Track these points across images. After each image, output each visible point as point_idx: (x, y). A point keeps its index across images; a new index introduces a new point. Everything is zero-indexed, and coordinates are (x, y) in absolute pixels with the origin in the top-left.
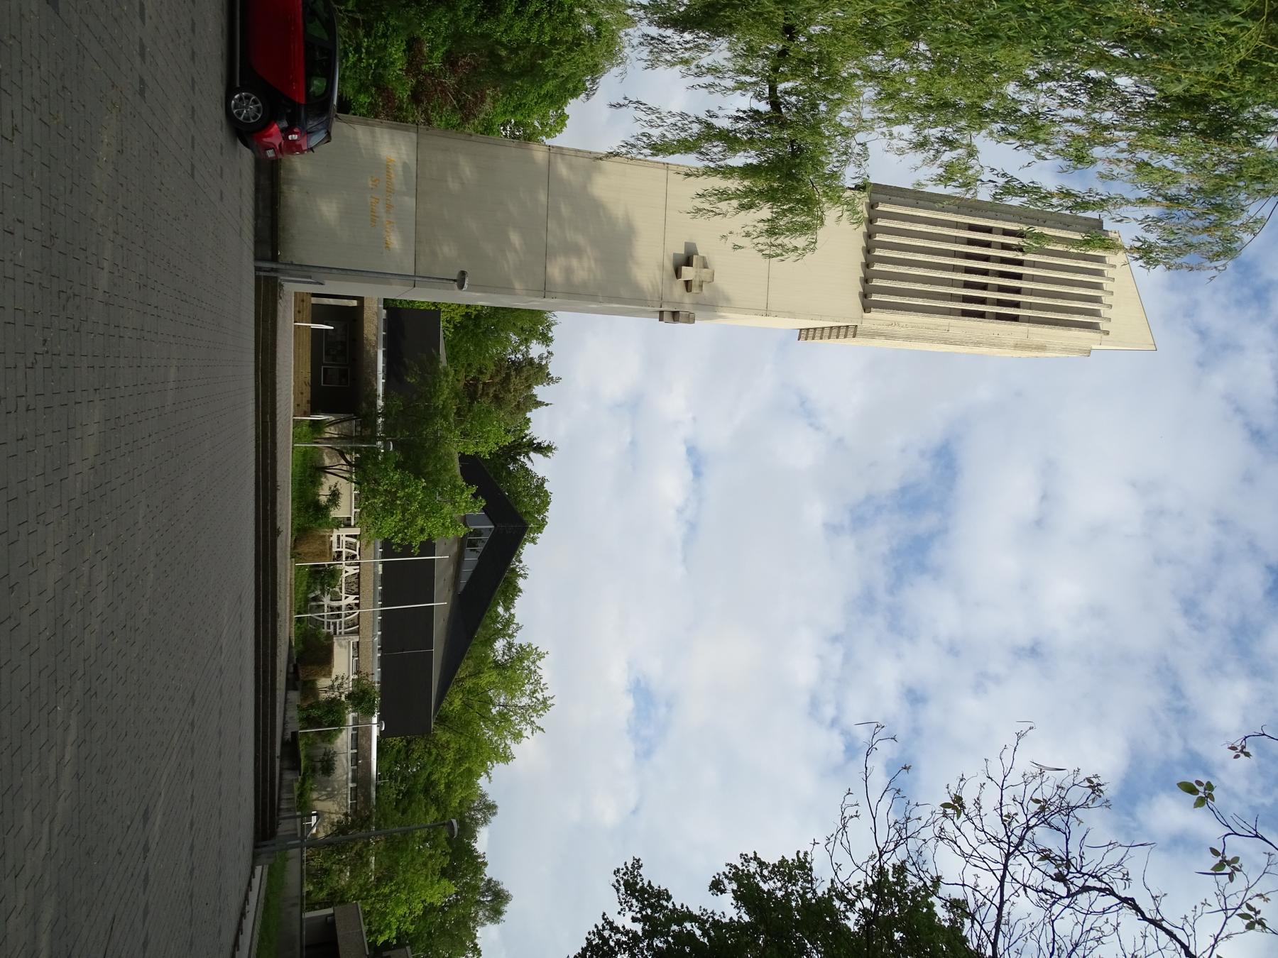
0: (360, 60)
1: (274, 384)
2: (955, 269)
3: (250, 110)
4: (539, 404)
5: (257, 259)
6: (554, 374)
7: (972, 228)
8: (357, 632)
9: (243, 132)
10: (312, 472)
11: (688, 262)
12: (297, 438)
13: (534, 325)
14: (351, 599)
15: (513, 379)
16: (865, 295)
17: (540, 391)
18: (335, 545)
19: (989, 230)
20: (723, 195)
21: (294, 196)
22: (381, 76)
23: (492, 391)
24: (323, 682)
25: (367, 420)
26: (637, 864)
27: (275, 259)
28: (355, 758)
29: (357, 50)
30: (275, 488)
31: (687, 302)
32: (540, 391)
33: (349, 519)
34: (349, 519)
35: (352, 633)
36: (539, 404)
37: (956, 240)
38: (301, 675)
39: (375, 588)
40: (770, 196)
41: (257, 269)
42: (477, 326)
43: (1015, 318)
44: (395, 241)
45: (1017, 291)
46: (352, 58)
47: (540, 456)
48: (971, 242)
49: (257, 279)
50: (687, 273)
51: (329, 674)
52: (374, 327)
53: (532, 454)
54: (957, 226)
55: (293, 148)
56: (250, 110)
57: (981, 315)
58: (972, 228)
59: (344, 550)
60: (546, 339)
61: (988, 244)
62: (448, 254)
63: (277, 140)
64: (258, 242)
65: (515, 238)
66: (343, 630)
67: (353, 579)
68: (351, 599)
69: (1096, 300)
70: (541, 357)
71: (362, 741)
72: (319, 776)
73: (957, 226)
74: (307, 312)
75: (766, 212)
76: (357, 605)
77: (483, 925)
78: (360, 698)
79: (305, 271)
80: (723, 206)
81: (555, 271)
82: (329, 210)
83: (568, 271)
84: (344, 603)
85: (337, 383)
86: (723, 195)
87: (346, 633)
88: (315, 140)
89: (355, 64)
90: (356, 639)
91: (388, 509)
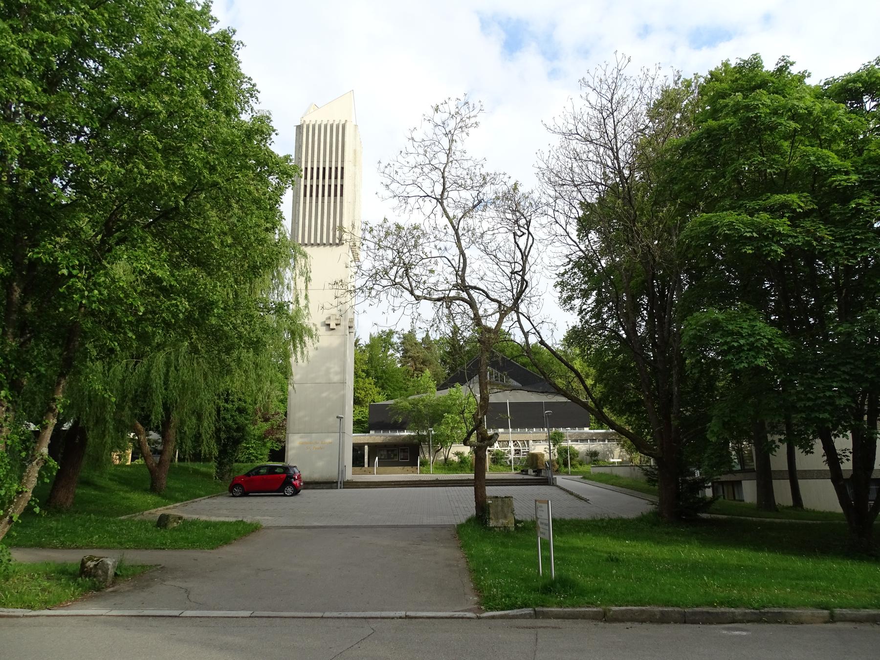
1: (800, 499)
2: (323, 202)
3: (290, 490)
7: (305, 195)
8: (528, 441)
9: (296, 492)
10: (447, 464)
11: (329, 325)
12: (428, 472)
14: (511, 444)
16: (337, 245)
19: (305, 186)
20: (302, 353)
21: (317, 476)
22: (259, 437)
23: (418, 366)
24: (547, 457)
25: (422, 439)
27: (337, 482)
28: (592, 440)
29: (248, 448)
31: (345, 324)
37: (311, 202)
40: (301, 337)
42: (381, 378)
43: (342, 168)
44: (329, 440)
45: (330, 169)
46: (252, 451)
48: (311, 195)
50: (333, 326)
51: (543, 455)
52: (375, 437)
54: (305, 203)
55: (299, 477)
56: (290, 490)
57: (342, 186)
58: (305, 195)
60: (391, 333)
61: (311, 186)
62: (332, 420)
63: (298, 482)
64: (332, 488)
65: (324, 395)
68: (511, 444)
69: (332, 126)
70: (399, 338)
71: (584, 437)
72: (600, 457)
73: (305, 203)
74: (370, 469)
75: (306, 338)
78: (555, 439)
79: (342, 471)
80: (305, 353)
81: (336, 378)
82: (320, 464)
83: (337, 373)
85: (406, 454)
86: (302, 353)
88: (296, 471)
90: (531, 442)
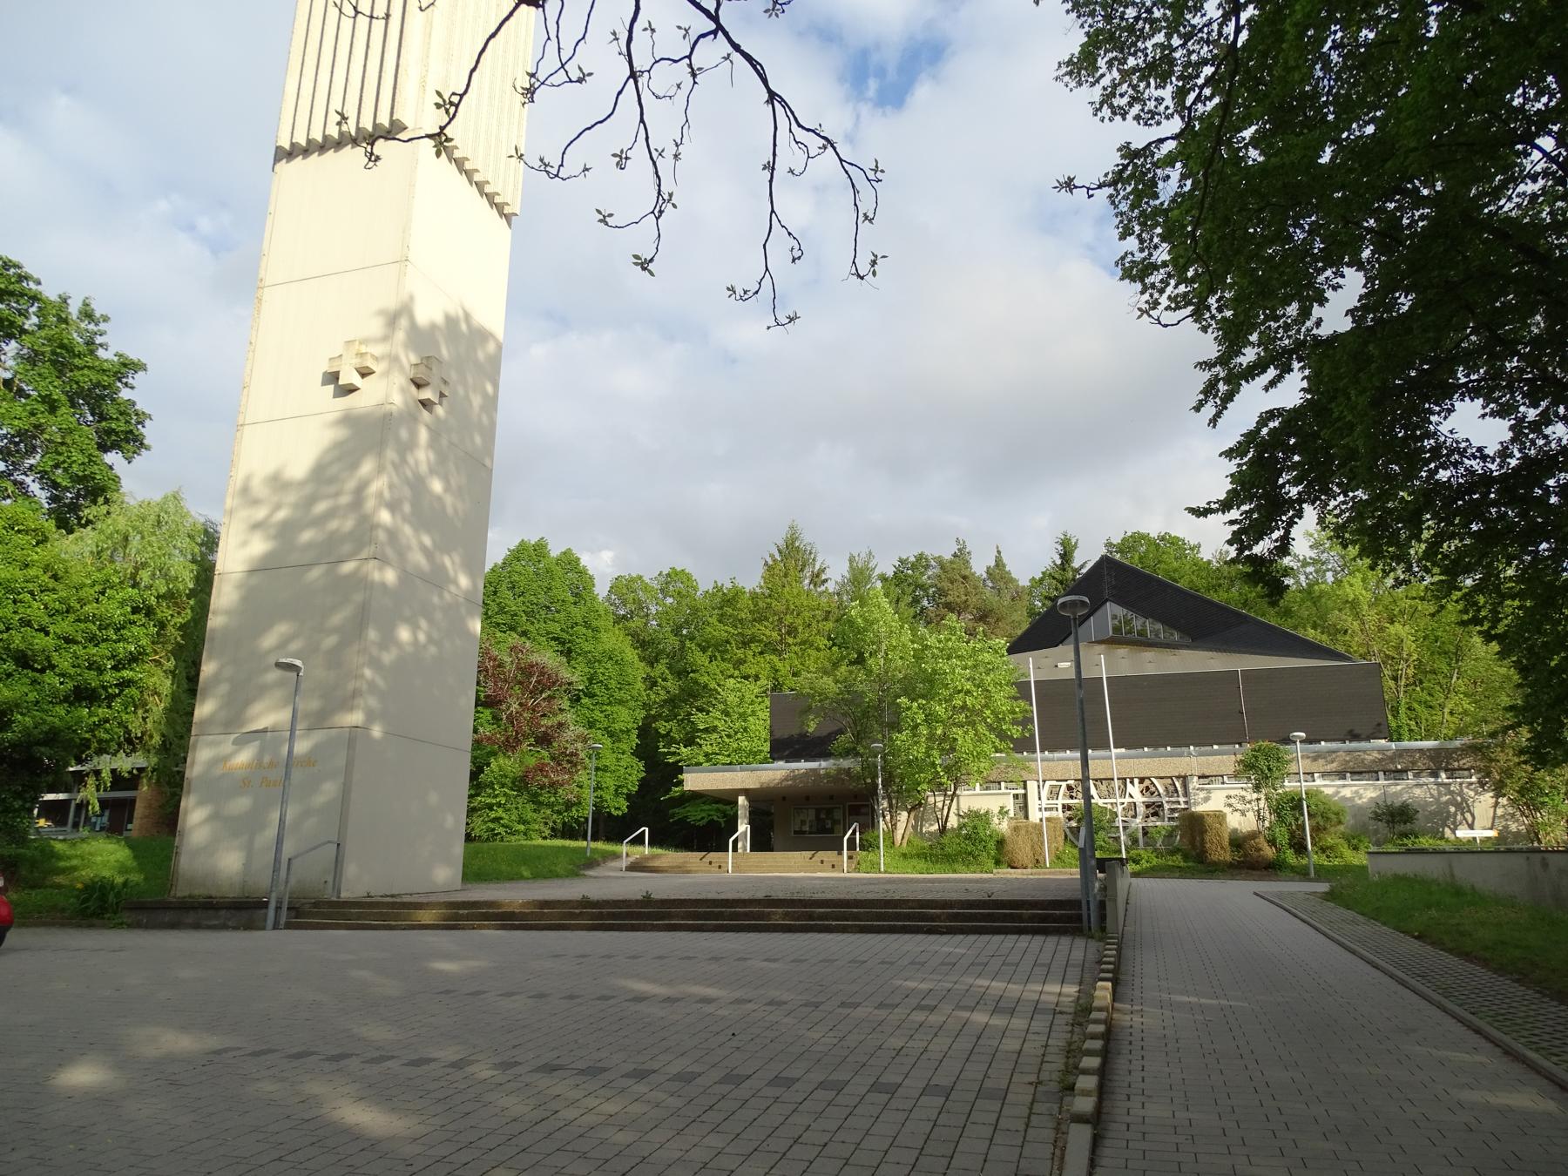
0: (499, 805)
4: (999, 563)
5: (264, 928)
6: (955, 549)
8: (1184, 779)
13: (532, 592)
14: (1134, 790)
15: (950, 599)
17: (980, 565)
18: (1054, 814)
26: (137, 367)
30: (647, 901)
32: (980, 565)
33: (1016, 796)
34: (1016, 796)
35: (1185, 786)
36: (999, 563)
38: (1227, 856)
39: (1171, 755)
41: (276, 927)
47: (1076, 554)
49: (288, 926)
53: (1076, 565)
59: (1062, 801)
66: (1182, 799)
67: (1103, 787)
76: (1142, 780)
77: (940, 561)
84: (1139, 799)
87: (1186, 794)
89: (506, 810)
90: (1194, 783)
91: (948, 745)
